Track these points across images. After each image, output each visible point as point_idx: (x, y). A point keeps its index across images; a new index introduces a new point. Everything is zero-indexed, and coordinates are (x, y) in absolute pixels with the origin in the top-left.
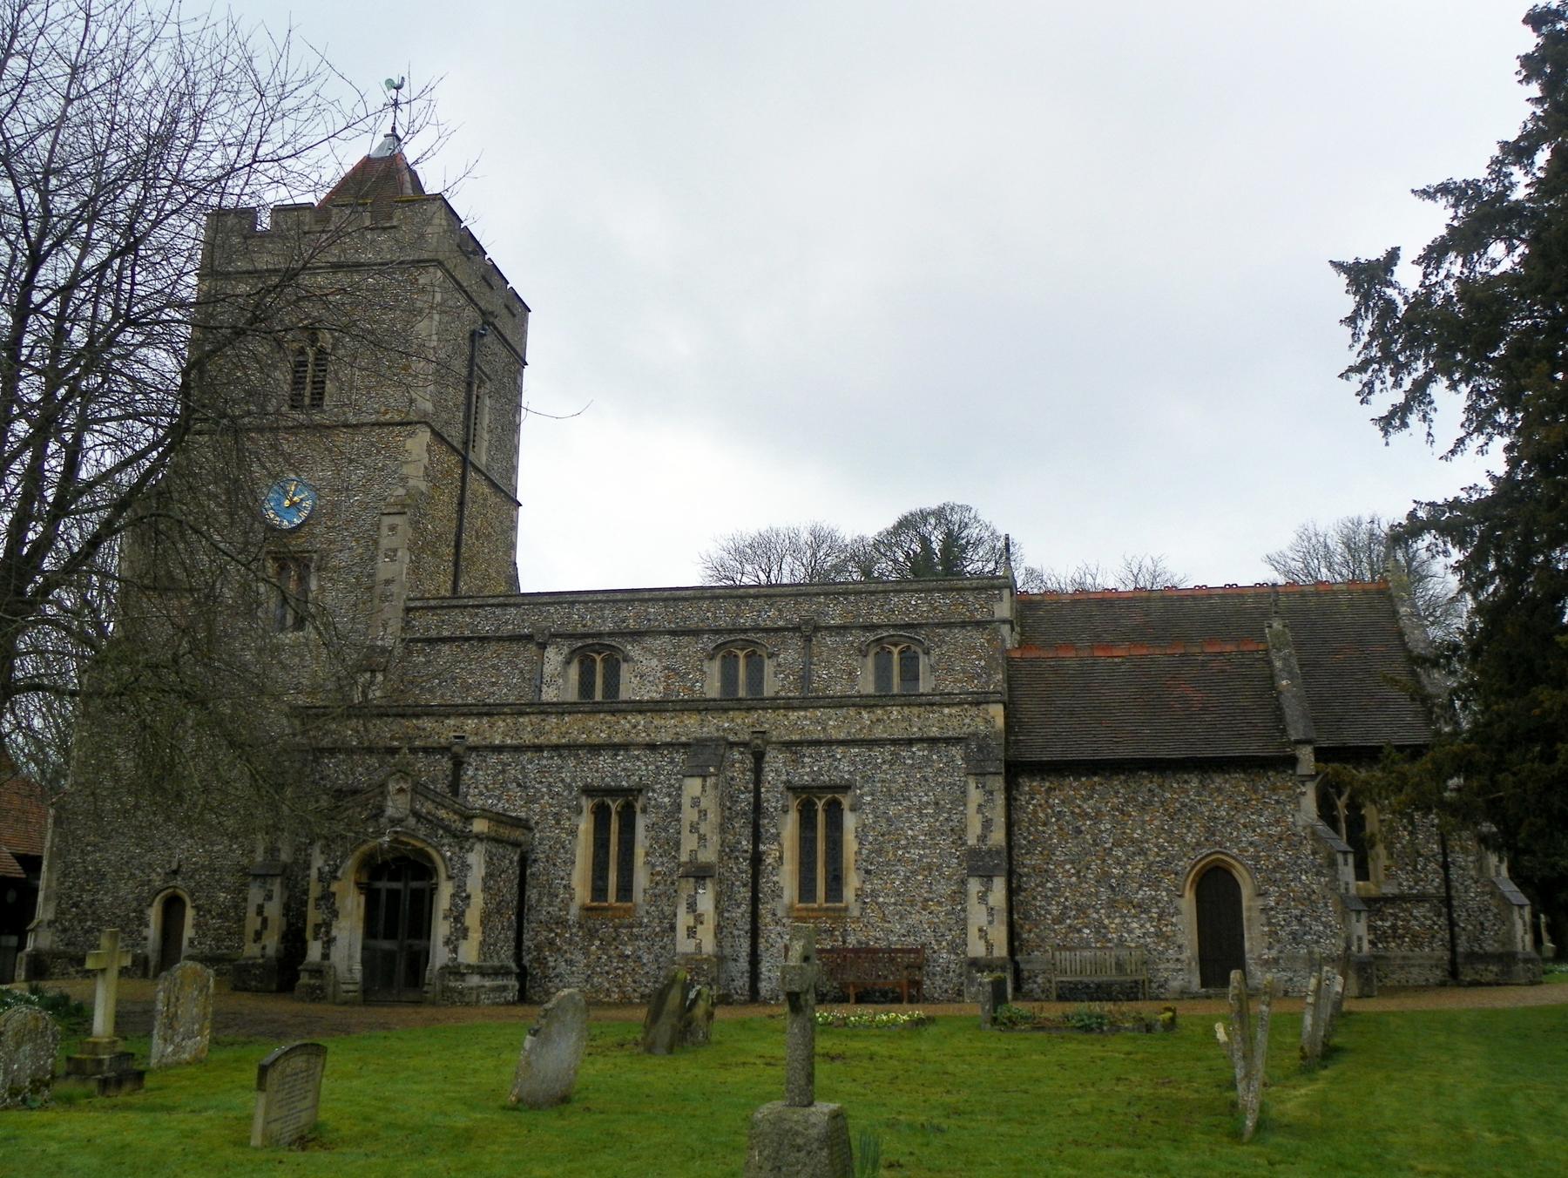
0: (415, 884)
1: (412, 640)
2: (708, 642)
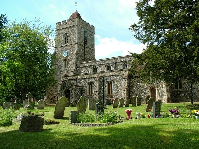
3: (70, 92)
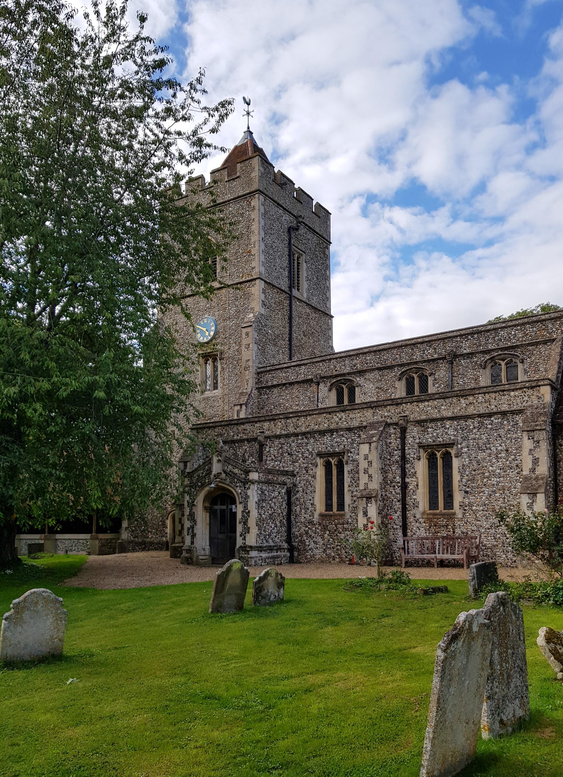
1: (261, 388)
2: (397, 371)
3: (233, 502)
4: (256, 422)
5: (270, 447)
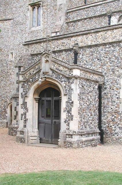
0: (55, 98)
4: (72, 37)
5: (83, 55)
